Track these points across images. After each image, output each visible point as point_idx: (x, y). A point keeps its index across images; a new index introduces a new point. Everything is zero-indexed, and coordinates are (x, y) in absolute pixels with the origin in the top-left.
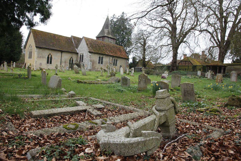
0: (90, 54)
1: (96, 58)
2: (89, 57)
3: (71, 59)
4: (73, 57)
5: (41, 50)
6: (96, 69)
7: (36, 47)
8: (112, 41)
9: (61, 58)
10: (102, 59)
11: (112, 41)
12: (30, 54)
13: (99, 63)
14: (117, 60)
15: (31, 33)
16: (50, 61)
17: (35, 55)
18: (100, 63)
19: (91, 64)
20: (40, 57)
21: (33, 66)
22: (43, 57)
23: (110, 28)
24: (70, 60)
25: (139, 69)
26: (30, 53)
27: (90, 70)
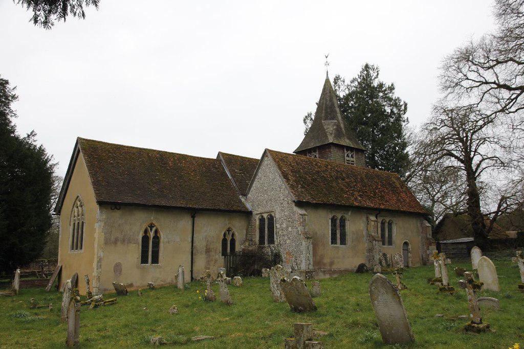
0: (302, 212)
1: (322, 222)
2: (297, 224)
3: (229, 238)
4: (234, 230)
5: (117, 214)
6: (324, 265)
7: (101, 203)
8: (354, 160)
9: (190, 236)
10: (343, 226)
11: (354, 160)
12: (78, 232)
13: (334, 241)
14: (390, 224)
15: (81, 154)
16: (153, 252)
17: (96, 235)
18: (338, 241)
19: (311, 247)
20: (116, 242)
21: (88, 283)
22: (126, 241)
23: (339, 115)
24: (224, 241)
25: (460, 246)
26: (78, 238)
27: (307, 273)
